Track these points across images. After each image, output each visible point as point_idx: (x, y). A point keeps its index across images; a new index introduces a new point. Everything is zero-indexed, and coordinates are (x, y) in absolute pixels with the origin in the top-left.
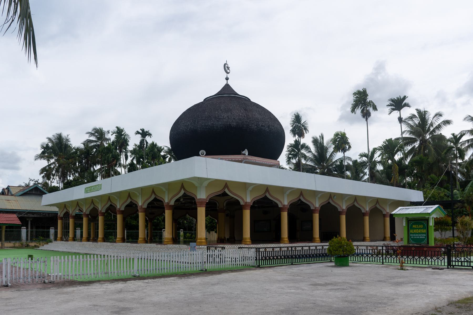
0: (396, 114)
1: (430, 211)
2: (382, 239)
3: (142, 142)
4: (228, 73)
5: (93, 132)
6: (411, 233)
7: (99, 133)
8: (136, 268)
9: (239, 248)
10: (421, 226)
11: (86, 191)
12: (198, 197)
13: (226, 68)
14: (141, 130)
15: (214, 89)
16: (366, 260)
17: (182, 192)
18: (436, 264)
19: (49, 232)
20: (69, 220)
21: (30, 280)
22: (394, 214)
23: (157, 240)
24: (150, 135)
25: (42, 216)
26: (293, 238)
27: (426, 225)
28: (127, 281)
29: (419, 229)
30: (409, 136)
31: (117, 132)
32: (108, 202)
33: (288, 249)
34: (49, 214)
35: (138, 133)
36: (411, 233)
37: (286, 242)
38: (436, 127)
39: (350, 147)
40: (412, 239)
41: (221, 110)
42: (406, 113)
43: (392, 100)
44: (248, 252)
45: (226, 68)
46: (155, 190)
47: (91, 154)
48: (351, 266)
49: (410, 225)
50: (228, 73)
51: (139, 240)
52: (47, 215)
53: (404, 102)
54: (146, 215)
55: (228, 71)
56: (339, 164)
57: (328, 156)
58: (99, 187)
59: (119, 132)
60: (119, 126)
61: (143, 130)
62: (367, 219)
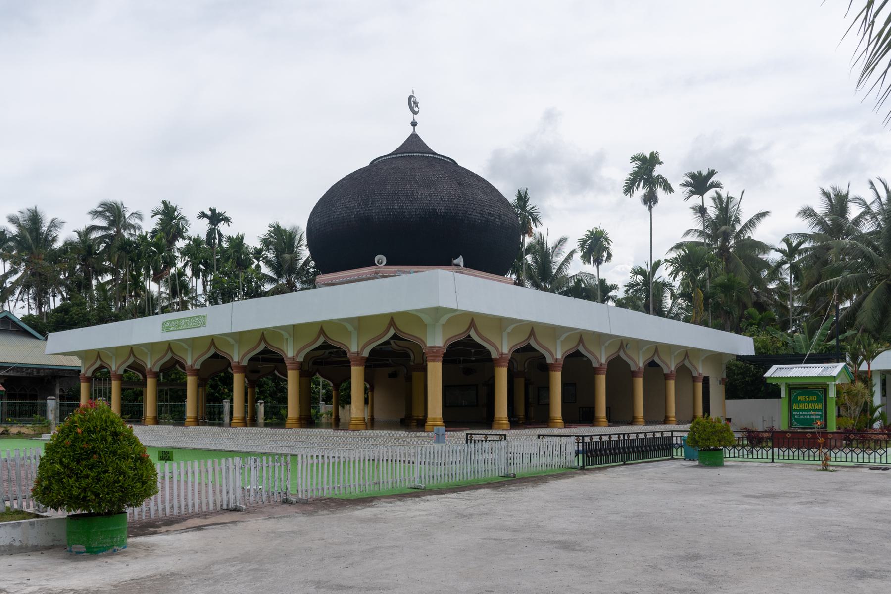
0: (696, 200)
1: (835, 372)
2: (690, 419)
3: (211, 233)
4: (415, 113)
5: (100, 209)
6: (795, 410)
7: (114, 213)
8: (417, 474)
9: (539, 436)
10: (814, 398)
11: (166, 327)
12: (429, 344)
13: (413, 104)
14: (210, 209)
15: (388, 142)
16: (732, 455)
17: (392, 332)
18: (872, 461)
19: (45, 405)
20: (110, 384)
21: (264, 498)
22: (770, 377)
23: (217, 421)
24: (227, 220)
25: (24, 374)
26: (612, 420)
27: (822, 396)
28: (371, 501)
29: (808, 402)
30: (698, 240)
31: (164, 213)
32: (209, 349)
33: (619, 437)
34: (38, 370)
35: (203, 215)
36: (795, 410)
37: (559, 425)
38: (746, 224)
39: (609, 256)
40: (796, 419)
41: (416, 182)
42: (708, 199)
43: (692, 176)
44: (559, 443)
45: (413, 104)
46: (324, 328)
47: (95, 254)
48: (727, 466)
49: (793, 396)
50: (415, 113)
51: (289, 421)
52: (35, 373)
53: (710, 181)
54: (246, 376)
55: (416, 110)
56: (573, 283)
57: (554, 271)
58: (202, 321)
59: (168, 213)
60: (167, 200)
61: (213, 211)
62: (639, 383)
